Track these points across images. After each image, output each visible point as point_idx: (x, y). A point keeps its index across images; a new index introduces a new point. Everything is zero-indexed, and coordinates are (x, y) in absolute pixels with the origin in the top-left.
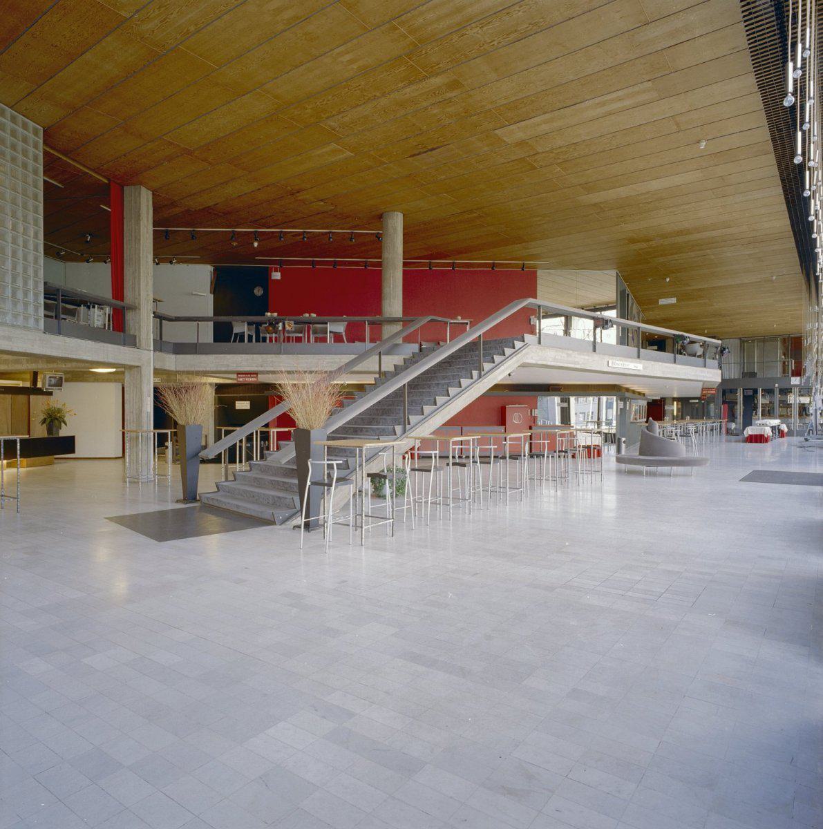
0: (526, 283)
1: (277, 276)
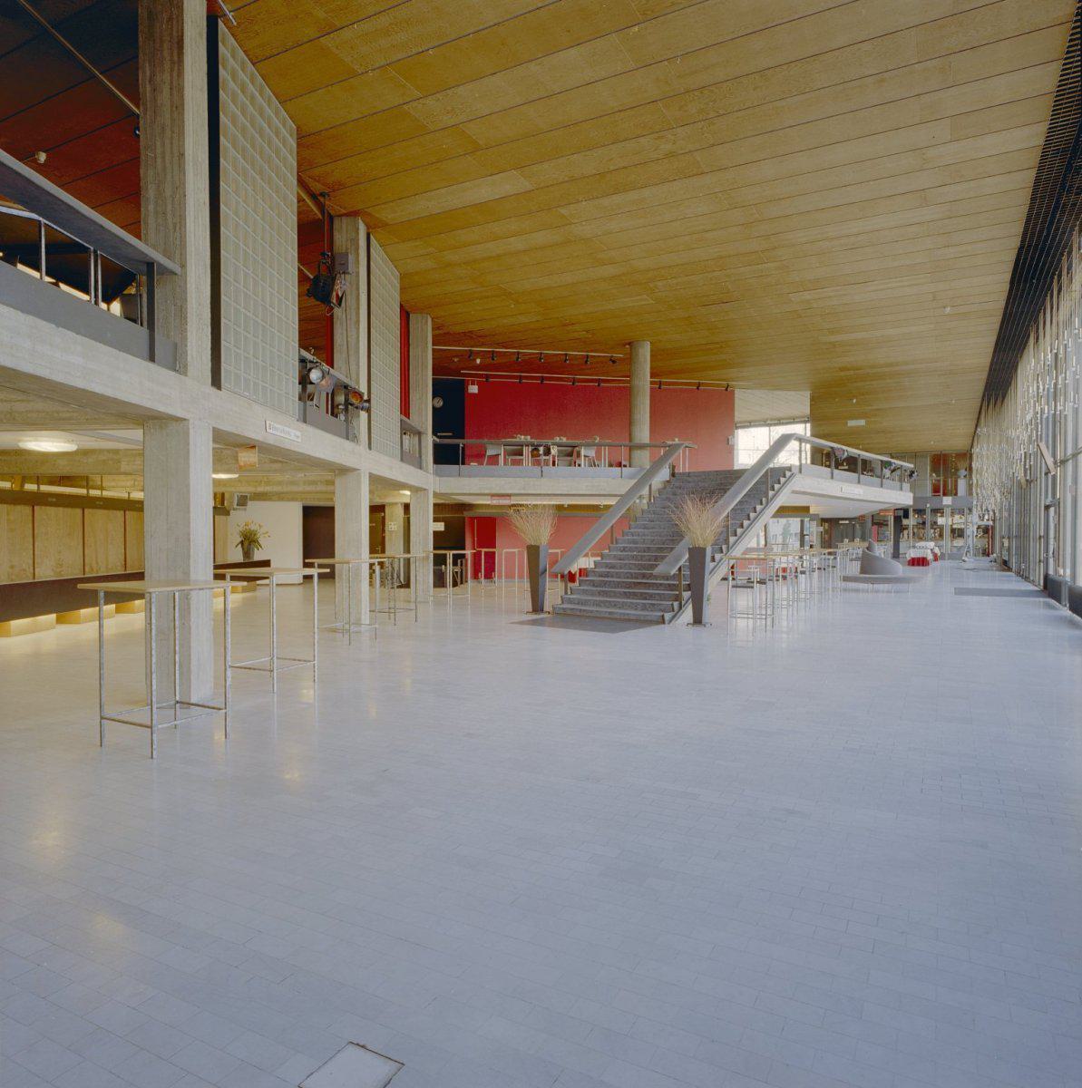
0: (725, 398)
1: (474, 389)
